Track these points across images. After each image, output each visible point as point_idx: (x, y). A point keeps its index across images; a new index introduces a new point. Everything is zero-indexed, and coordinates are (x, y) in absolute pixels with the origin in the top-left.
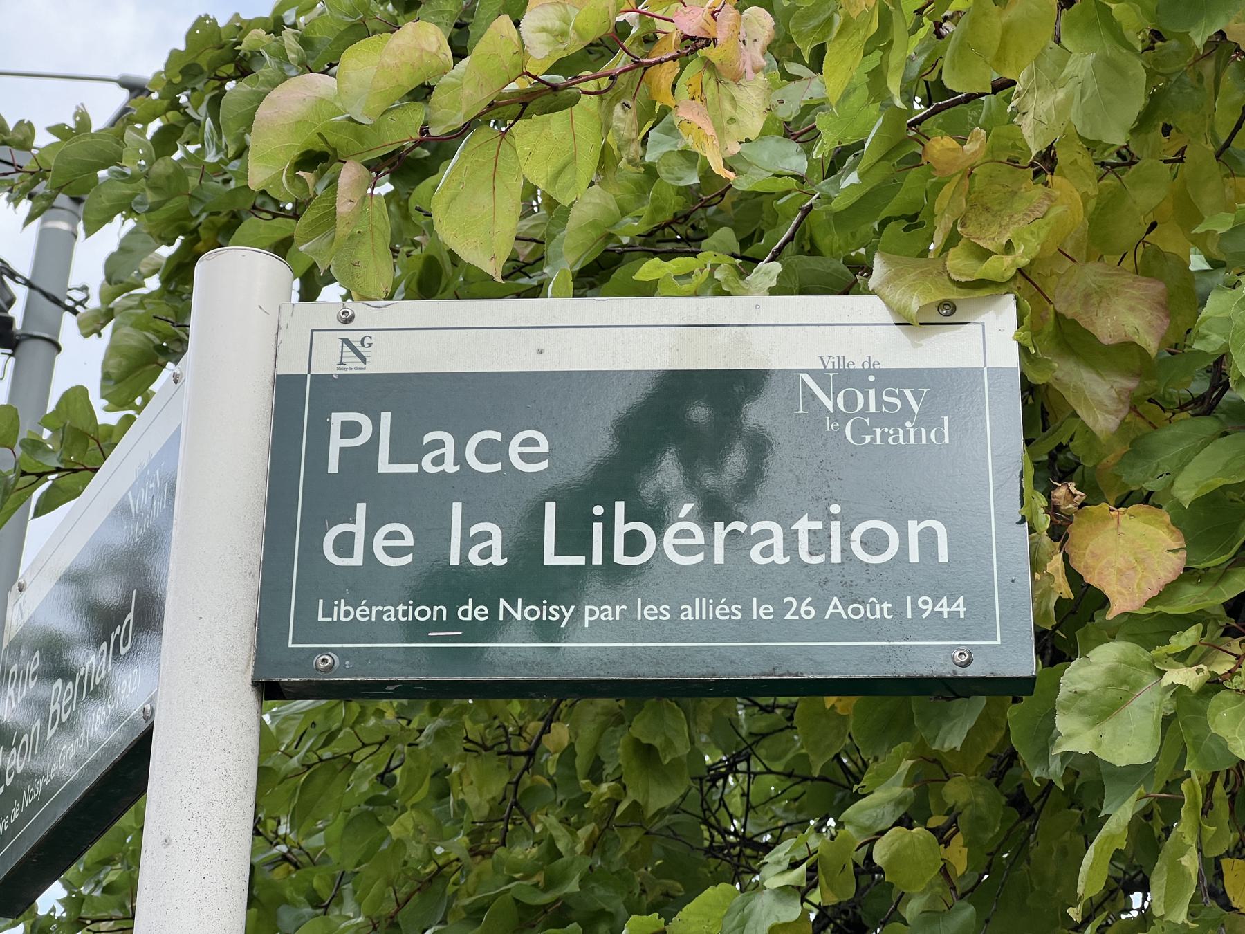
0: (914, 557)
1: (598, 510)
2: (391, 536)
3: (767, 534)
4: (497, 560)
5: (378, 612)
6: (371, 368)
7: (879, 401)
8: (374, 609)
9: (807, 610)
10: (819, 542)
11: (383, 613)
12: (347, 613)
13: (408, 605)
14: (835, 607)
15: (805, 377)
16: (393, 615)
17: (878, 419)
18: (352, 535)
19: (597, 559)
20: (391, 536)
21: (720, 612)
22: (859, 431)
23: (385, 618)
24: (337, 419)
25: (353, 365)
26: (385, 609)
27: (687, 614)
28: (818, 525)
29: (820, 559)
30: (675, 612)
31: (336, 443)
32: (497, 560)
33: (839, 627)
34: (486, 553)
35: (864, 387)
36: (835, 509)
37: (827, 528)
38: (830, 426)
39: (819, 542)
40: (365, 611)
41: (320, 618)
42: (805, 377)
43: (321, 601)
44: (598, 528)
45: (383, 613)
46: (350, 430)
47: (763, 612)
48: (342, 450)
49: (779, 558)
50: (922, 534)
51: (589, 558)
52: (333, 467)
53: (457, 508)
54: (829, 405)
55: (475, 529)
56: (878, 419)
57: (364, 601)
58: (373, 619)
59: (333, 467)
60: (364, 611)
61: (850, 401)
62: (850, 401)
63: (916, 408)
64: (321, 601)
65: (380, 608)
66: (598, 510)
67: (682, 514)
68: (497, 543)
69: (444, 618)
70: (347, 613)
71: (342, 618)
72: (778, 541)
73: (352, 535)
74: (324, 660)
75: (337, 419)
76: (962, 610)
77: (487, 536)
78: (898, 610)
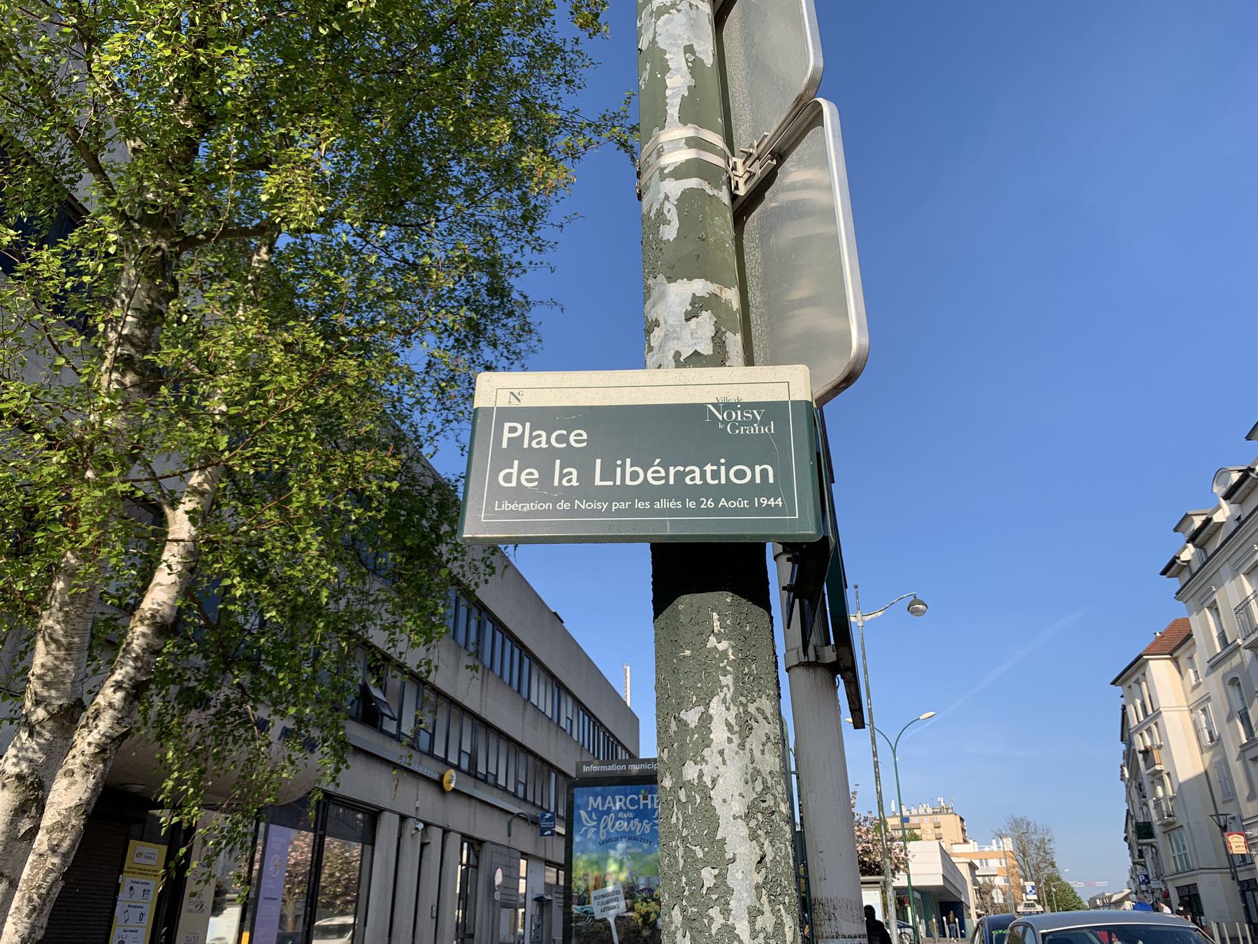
0: (758, 481)
1: (619, 462)
2: (529, 474)
3: (693, 472)
4: (575, 483)
5: (677, 473)
6: (522, 405)
7: (742, 416)
8: (672, 470)
9: (711, 504)
10: (715, 475)
11: (685, 474)
12: (634, 476)
13: (719, 465)
14: (723, 502)
15: (710, 406)
16: (698, 478)
17: (742, 423)
18: (511, 474)
19: (618, 483)
20: (529, 474)
21: (672, 505)
22: (733, 429)
23: (687, 480)
24: (507, 425)
25: (515, 403)
26: (687, 469)
27: (657, 506)
28: (715, 468)
29: (717, 482)
30: (652, 505)
31: (506, 435)
32: (575, 483)
33: (725, 511)
34: (569, 481)
35: (736, 410)
36: (723, 461)
37: (719, 470)
38: (720, 426)
39: (715, 475)
40: (659, 472)
41: (598, 482)
42: (710, 406)
43: (598, 461)
44: (619, 470)
45: (685, 474)
46: (513, 430)
47: (691, 505)
48: (509, 439)
49: (698, 481)
50: (762, 471)
51: (615, 482)
52: (504, 445)
53: (558, 462)
54: (720, 418)
55: (565, 471)
56: (742, 423)
57: (658, 461)
58: (672, 482)
59: (504, 445)
60: (658, 472)
61: (729, 416)
62: (729, 416)
63: (759, 418)
64: (598, 461)
65: (681, 468)
66: (619, 462)
67: (656, 463)
68: (574, 476)
69: (771, 480)
70: (634, 476)
71: (628, 482)
72: (697, 474)
73: (511, 474)
74: (433, 512)
75: (507, 425)
76: (780, 503)
77: (571, 473)
78: (751, 503)
